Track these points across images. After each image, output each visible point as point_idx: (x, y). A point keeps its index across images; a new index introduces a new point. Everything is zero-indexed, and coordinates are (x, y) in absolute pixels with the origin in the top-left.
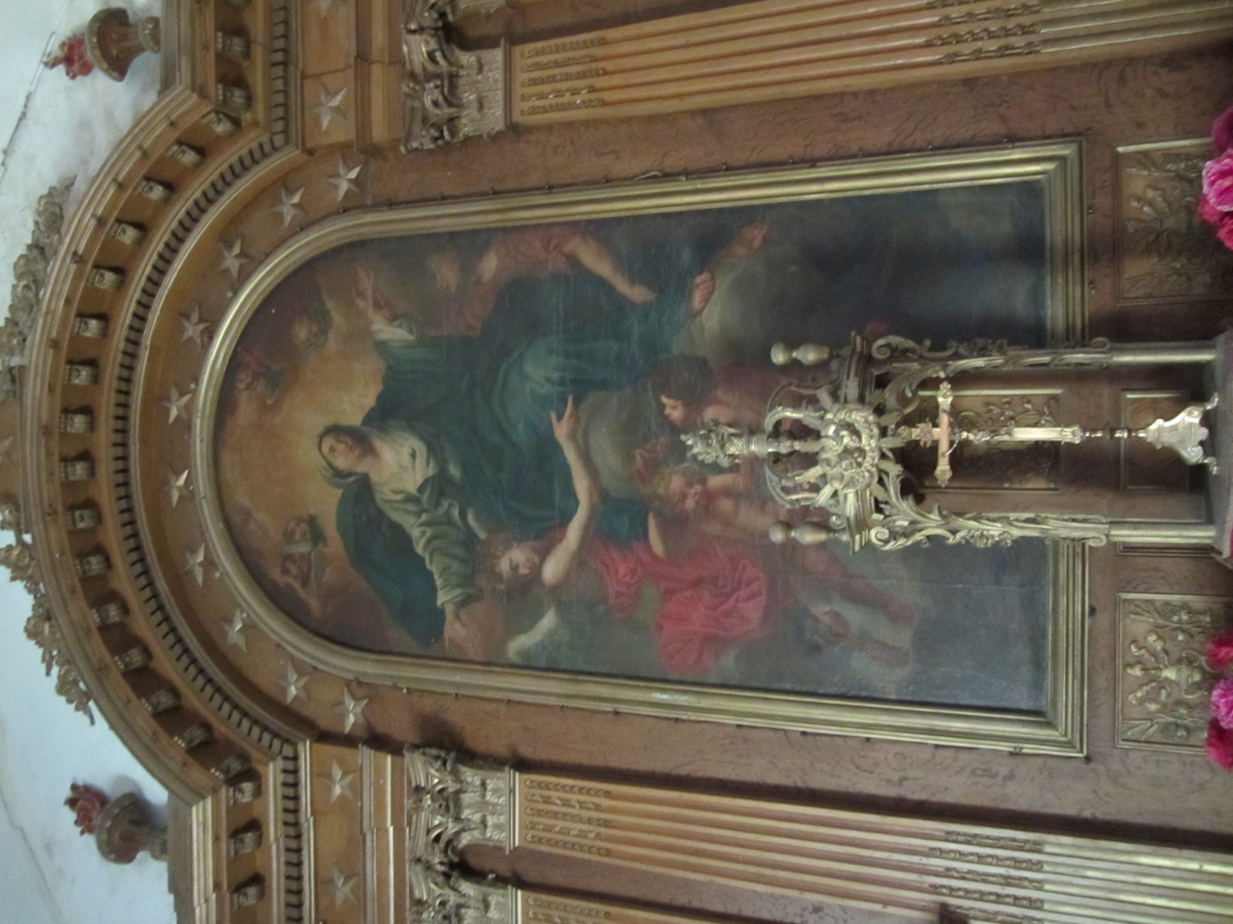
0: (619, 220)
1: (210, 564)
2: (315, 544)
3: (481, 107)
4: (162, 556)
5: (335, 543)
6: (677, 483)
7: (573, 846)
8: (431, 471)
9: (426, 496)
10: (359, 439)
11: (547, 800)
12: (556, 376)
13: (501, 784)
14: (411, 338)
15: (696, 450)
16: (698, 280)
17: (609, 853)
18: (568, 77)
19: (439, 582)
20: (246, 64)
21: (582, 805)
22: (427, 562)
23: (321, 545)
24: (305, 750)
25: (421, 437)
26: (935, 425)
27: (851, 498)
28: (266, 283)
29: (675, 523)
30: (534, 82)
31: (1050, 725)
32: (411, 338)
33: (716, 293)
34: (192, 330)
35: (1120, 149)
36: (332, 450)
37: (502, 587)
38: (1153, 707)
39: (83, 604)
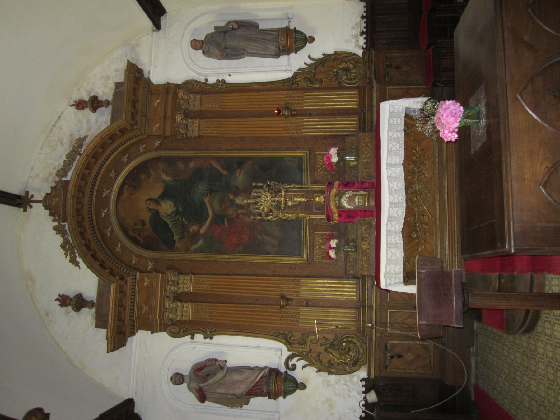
0: (222, 157)
1: (112, 231)
2: (143, 226)
3: (193, 132)
4: (99, 230)
5: (148, 225)
6: (231, 211)
7: (205, 290)
8: (175, 209)
9: (173, 215)
10: (157, 202)
11: (199, 281)
12: (205, 189)
13: (188, 278)
14: (171, 179)
15: (237, 202)
16: (238, 171)
17: (213, 291)
18: (212, 127)
19: (175, 234)
20: (136, 115)
21: (208, 281)
22: (172, 230)
23: (144, 226)
24: (138, 274)
25: (173, 201)
26: (281, 198)
27: (266, 208)
28: (134, 165)
29: (230, 220)
30: (205, 127)
31: (302, 257)
32: (171, 179)
33: (241, 174)
34: (112, 175)
35: (316, 152)
36: (149, 204)
37: (190, 235)
38: (320, 253)
39: (80, 239)
